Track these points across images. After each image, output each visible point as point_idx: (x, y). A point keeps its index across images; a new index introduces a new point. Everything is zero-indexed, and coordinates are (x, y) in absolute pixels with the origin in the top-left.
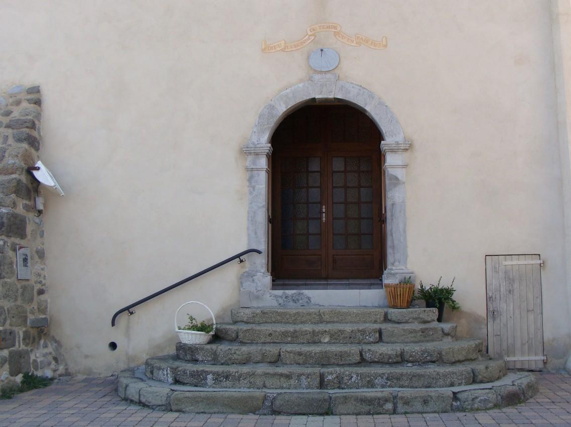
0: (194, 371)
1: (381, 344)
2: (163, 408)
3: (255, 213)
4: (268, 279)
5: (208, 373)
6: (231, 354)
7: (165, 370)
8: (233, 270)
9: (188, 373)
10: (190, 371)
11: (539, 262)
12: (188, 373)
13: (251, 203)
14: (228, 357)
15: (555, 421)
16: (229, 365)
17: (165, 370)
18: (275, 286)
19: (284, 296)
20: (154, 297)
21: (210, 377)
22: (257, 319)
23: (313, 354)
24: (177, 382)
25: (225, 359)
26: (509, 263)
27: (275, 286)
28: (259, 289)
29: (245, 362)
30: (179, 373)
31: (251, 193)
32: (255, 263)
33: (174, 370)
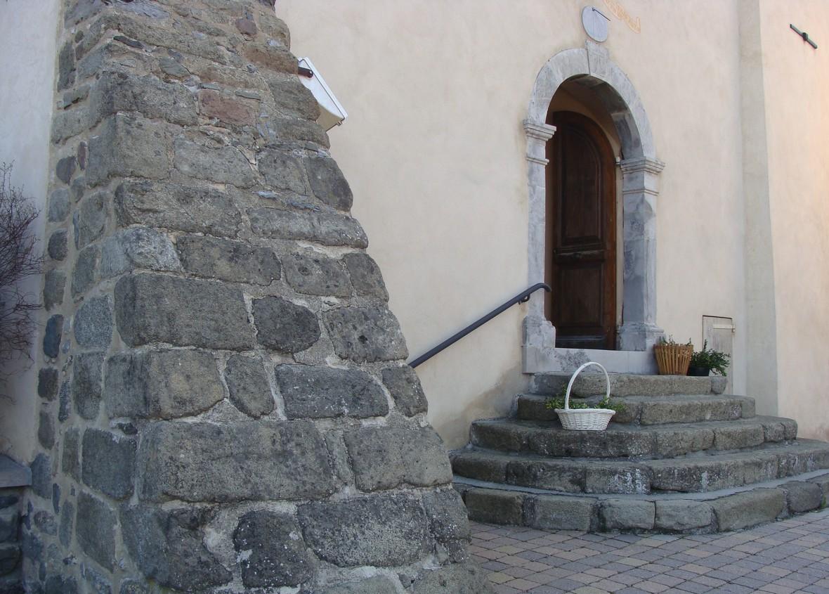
0: (684, 470)
1: (468, 440)
2: (708, 529)
3: (535, 227)
4: (550, 331)
5: (701, 470)
6: (678, 441)
7: (629, 474)
8: (514, 313)
9: (676, 473)
10: (678, 470)
11: (730, 327)
12: (676, 473)
13: (531, 212)
14: (674, 447)
15: (241, 592)
16: (673, 458)
17: (629, 474)
18: (558, 345)
19: (568, 357)
20: (436, 353)
21: (705, 475)
22: (624, 390)
23: (563, 450)
24: (654, 489)
25: (669, 449)
26: (716, 326)
27: (558, 345)
28: (545, 345)
29: (711, 447)
30: (660, 475)
31: (531, 196)
32: (535, 306)
33: (649, 472)
